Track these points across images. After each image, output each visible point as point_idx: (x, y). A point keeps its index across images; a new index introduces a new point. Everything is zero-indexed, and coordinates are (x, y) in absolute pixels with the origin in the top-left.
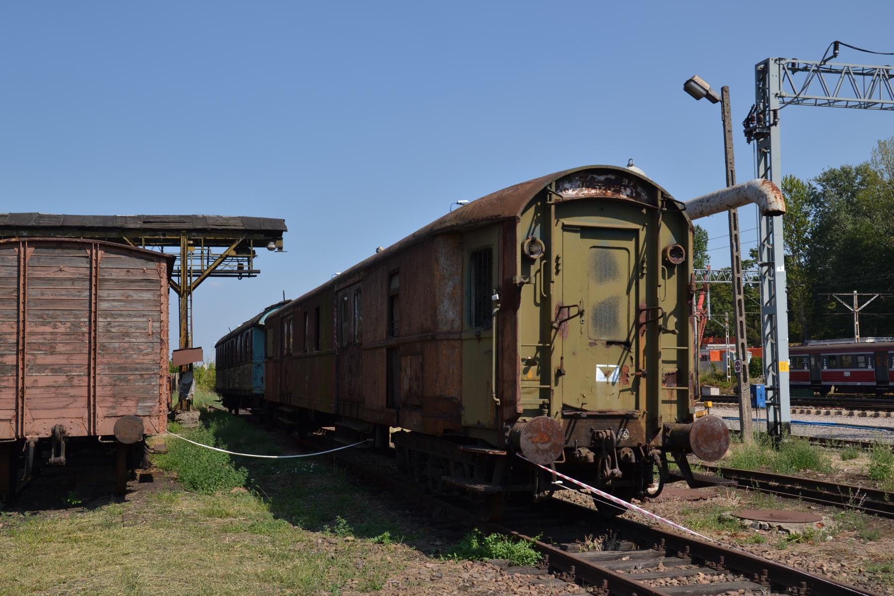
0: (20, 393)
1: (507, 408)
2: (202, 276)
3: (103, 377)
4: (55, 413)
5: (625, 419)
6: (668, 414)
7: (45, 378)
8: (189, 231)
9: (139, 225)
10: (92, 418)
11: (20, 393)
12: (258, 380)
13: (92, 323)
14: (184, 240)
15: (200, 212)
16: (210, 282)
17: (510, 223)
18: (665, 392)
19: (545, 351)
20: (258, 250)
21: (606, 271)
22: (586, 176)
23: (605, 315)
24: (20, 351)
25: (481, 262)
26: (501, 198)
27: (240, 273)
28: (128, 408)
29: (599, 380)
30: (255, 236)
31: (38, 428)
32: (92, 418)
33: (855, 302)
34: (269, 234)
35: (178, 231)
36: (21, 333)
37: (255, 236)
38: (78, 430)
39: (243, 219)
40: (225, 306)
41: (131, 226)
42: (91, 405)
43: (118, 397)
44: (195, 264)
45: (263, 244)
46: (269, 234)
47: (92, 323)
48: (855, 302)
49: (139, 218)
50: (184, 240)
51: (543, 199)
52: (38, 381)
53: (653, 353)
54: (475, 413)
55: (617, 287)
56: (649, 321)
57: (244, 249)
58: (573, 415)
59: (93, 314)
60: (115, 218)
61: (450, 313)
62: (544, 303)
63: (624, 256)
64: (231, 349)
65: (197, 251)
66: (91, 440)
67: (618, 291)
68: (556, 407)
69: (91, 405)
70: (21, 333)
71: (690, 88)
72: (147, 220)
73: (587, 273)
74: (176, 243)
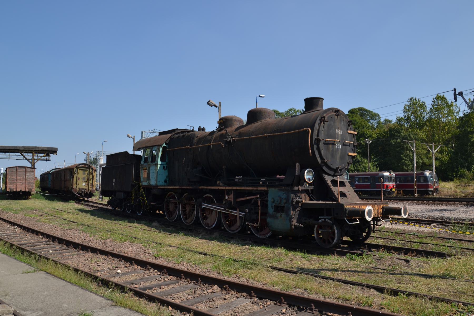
0: (16, 185)
1: (72, 188)
2: (37, 160)
3: (27, 183)
4: (21, 188)
5: (86, 189)
6: (90, 189)
7: (19, 184)
8: (35, 150)
9: (23, 149)
10: (25, 189)
11: (16, 185)
12: (49, 185)
13: (26, 177)
14: (33, 152)
15: (37, 146)
16: (39, 161)
17: (73, 169)
18: (90, 186)
19: (77, 182)
20: (51, 155)
21: (84, 174)
22: (82, 164)
23: (84, 178)
24: (16, 180)
25: (71, 172)
26: (73, 166)
27: (47, 160)
28: (30, 188)
29: (83, 185)
30: (49, 152)
31: (19, 190)
32: (25, 189)
33: (434, 148)
34: (54, 151)
35: (32, 151)
36: (16, 178)
37: (49, 152)
38: (23, 190)
39: (48, 148)
40: (43, 167)
41: (21, 149)
42: (25, 187)
43: (29, 186)
44: (36, 158)
45: (52, 153)
46: (54, 151)
47: (26, 177)
48: (434, 148)
49: (23, 147)
50: (33, 152)
51: (77, 167)
52: (19, 184)
53: (89, 182)
54: (70, 189)
55: (85, 175)
56: (89, 179)
57: (48, 155)
58: (80, 189)
59: (26, 176)
60: (17, 147)
61: (68, 178)
62: (77, 177)
63: (86, 172)
64: (44, 177)
65: (36, 155)
66: (25, 191)
67: (86, 176)
68: (78, 188)
69: (25, 187)
70: (16, 178)
71: (128, 136)
72: (25, 147)
73: (81, 174)
74: (32, 153)
